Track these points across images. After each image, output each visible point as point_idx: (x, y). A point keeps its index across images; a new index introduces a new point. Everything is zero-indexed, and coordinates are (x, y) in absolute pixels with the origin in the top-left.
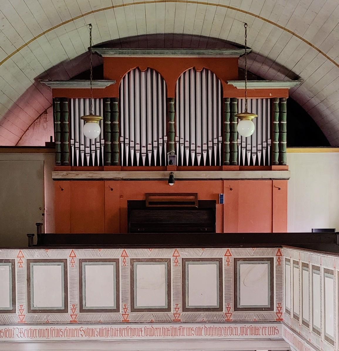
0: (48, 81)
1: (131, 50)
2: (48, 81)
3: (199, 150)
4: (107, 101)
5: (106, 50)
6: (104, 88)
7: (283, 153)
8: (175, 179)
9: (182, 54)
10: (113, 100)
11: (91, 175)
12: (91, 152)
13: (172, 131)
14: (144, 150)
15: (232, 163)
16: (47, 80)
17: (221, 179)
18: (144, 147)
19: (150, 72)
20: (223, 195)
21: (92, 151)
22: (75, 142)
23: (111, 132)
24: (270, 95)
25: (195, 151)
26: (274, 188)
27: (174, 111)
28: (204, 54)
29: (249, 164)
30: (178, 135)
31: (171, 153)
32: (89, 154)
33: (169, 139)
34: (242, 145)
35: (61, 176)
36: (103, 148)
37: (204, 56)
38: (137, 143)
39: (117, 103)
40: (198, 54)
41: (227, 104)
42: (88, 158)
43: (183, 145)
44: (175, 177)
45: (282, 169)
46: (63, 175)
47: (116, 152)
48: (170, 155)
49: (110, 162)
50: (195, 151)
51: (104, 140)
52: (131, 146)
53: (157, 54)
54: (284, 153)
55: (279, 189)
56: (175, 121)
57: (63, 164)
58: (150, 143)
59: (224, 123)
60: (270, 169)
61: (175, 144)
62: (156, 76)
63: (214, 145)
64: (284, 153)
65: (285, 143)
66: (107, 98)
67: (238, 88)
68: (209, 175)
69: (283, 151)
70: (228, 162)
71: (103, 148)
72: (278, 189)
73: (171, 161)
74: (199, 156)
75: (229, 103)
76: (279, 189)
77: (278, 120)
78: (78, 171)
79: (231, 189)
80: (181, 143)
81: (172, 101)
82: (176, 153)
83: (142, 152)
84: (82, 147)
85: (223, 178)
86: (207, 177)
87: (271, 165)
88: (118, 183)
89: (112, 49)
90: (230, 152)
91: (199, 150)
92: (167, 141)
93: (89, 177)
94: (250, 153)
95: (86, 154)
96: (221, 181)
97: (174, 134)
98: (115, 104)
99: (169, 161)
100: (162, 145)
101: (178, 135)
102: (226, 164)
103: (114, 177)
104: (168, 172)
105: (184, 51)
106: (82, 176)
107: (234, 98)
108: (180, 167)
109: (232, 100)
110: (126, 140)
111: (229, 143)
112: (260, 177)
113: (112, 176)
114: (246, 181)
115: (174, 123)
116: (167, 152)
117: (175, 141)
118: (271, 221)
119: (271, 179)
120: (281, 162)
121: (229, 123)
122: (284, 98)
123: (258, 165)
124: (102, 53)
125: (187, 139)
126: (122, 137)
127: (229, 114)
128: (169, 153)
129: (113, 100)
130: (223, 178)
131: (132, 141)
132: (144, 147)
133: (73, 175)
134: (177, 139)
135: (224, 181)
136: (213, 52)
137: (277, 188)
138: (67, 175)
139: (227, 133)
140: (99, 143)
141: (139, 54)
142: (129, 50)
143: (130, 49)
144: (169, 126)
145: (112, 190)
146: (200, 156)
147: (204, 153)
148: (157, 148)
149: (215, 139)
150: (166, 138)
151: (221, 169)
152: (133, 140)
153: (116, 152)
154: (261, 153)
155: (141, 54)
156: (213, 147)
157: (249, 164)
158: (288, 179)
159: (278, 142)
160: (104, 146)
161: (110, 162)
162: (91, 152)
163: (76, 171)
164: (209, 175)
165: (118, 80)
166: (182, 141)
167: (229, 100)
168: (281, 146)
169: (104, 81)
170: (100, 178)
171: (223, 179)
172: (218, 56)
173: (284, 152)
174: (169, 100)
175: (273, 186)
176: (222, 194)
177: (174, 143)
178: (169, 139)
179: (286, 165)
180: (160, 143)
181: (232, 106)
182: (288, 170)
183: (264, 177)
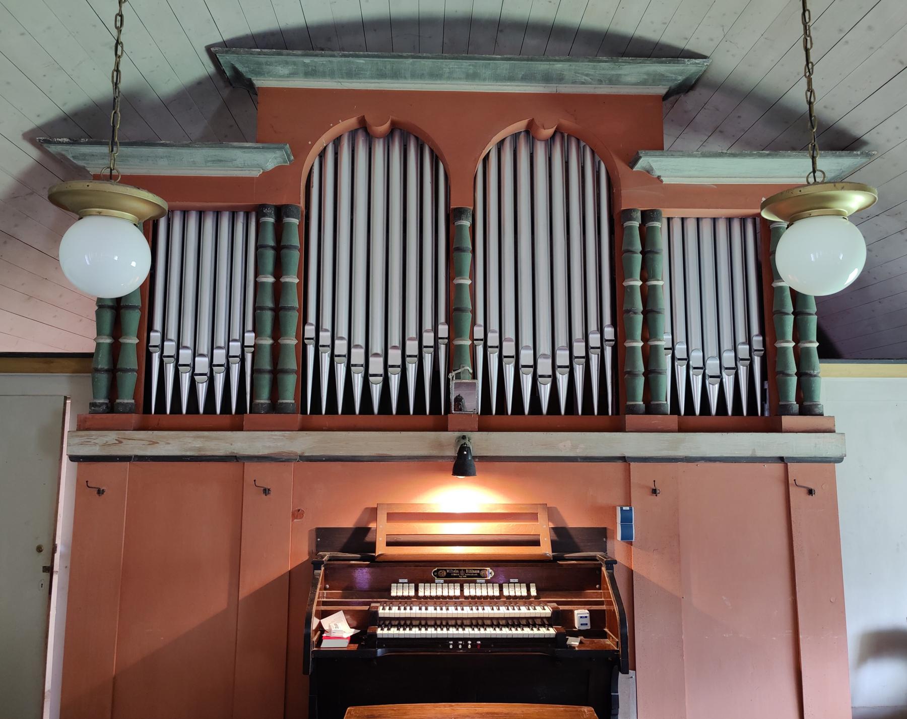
0: (67, 143)
1: (339, 59)
2: (67, 143)
3: (544, 367)
4: (265, 215)
5: (262, 59)
6: (256, 173)
8: (474, 457)
9: (497, 78)
10: (281, 212)
11: (198, 444)
12: (212, 371)
13: (465, 306)
14: (376, 366)
15: (651, 408)
16: (66, 140)
17: (623, 459)
18: (376, 355)
20: (631, 510)
21: (215, 368)
22: (164, 338)
23: (275, 309)
25: (532, 370)
27: (470, 247)
28: (560, 79)
30: (480, 320)
31: (462, 376)
32: (205, 378)
33: (455, 330)
34: (676, 352)
35: (97, 448)
36: (249, 357)
37: (564, 89)
38: (356, 343)
39: (296, 221)
40: (547, 78)
41: (631, 228)
42: (202, 390)
43: (497, 350)
44: (475, 451)
45: (810, 428)
46: (106, 445)
47: (286, 372)
48: (459, 381)
49: (267, 402)
50: (532, 370)
51: (253, 335)
52: (336, 353)
53: (421, 76)
56: (473, 276)
57: (112, 408)
58: (397, 344)
59: (625, 284)
61: (473, 348)
66: (264, 206)
67: (666, 180)
68: (582, 446)
70: (642, 403)
71: (249, 357)
73: (459, 400)
75: (636, 224)
78: (156, 432)
79: (654, 492)
80: (489, 344)
81: (463, 216)
82: (474, 376)
83: (371, 372)
84: (185, 356)
85: (628, 454)
86: (578, 451)
88: (288, 472)
89: (282, 55)
90: (644, 374)
91: (544, 367)
92: (448, 338)
93: (190, 450)
94: (700, 377)
95: (196, 377)
96: (620, 465)
97: (470, 315)
98: (289, 223)
99: (453, 397)
100: (432, 349)
101: (480, 320)
102: (633, 410)
103: (276, 451)
104: (449, 437)
105: (504, 66)
106: (169, 447)
107: (652, 211)
109: (648, 216)
110: (490, 335)
111: (640, 344)
112: (747, 453)
113: (270, 447)
114: (702, 465)
115: (469, 282)
116: (448, 370)
117: (473, 339)
119: (781, 459)
120: (807, 407)
121: (639, 283)
124: (254, 72)
125: (359, 338)
126: (311, 324)
127: (639, 257)
128: (454, 373)
129: (281, 212)
130: (627, 455)
131: (342, 338)
132: (376, 355)
133: (138, 443)
134: (479, 332)
136: (591, 72)
137: (802, 492)
138: (121, 442)
139: (635, 313)
140: (239, 344)
141: (365, 78)
142: (333, 56)
143: (335, 53)
144: (453, 291)
145: (266, 491)
146: (549, 386)
147: (559, 376)
148: (416, 359)
149: (593, 333)
150: (443, 330)
151: (619, 428)
152: (345, 335)
153: (286, 372)
154: (732, 378)
155: (372, 77)
156: (587, 358)
157: (698, 411)
158: (840, 460)
159: (793, 344)
161: (267, 402)
162: (212, 371)
163: (150, 432)
164: (582, 446)
165: (299, 151)
166: (493, 339)
168: (801, 356)
169: (249, 148)
170: (228, 453)
171: (629, 457)
172: (604, 90)
174: (453, 215)
175: (791, 481)
177: (469, 342)
178: (455, 330)
179: (822, 415)
180: (408, 352)
181: (647, 235)
182: (832, 431)
183: (760, 453)
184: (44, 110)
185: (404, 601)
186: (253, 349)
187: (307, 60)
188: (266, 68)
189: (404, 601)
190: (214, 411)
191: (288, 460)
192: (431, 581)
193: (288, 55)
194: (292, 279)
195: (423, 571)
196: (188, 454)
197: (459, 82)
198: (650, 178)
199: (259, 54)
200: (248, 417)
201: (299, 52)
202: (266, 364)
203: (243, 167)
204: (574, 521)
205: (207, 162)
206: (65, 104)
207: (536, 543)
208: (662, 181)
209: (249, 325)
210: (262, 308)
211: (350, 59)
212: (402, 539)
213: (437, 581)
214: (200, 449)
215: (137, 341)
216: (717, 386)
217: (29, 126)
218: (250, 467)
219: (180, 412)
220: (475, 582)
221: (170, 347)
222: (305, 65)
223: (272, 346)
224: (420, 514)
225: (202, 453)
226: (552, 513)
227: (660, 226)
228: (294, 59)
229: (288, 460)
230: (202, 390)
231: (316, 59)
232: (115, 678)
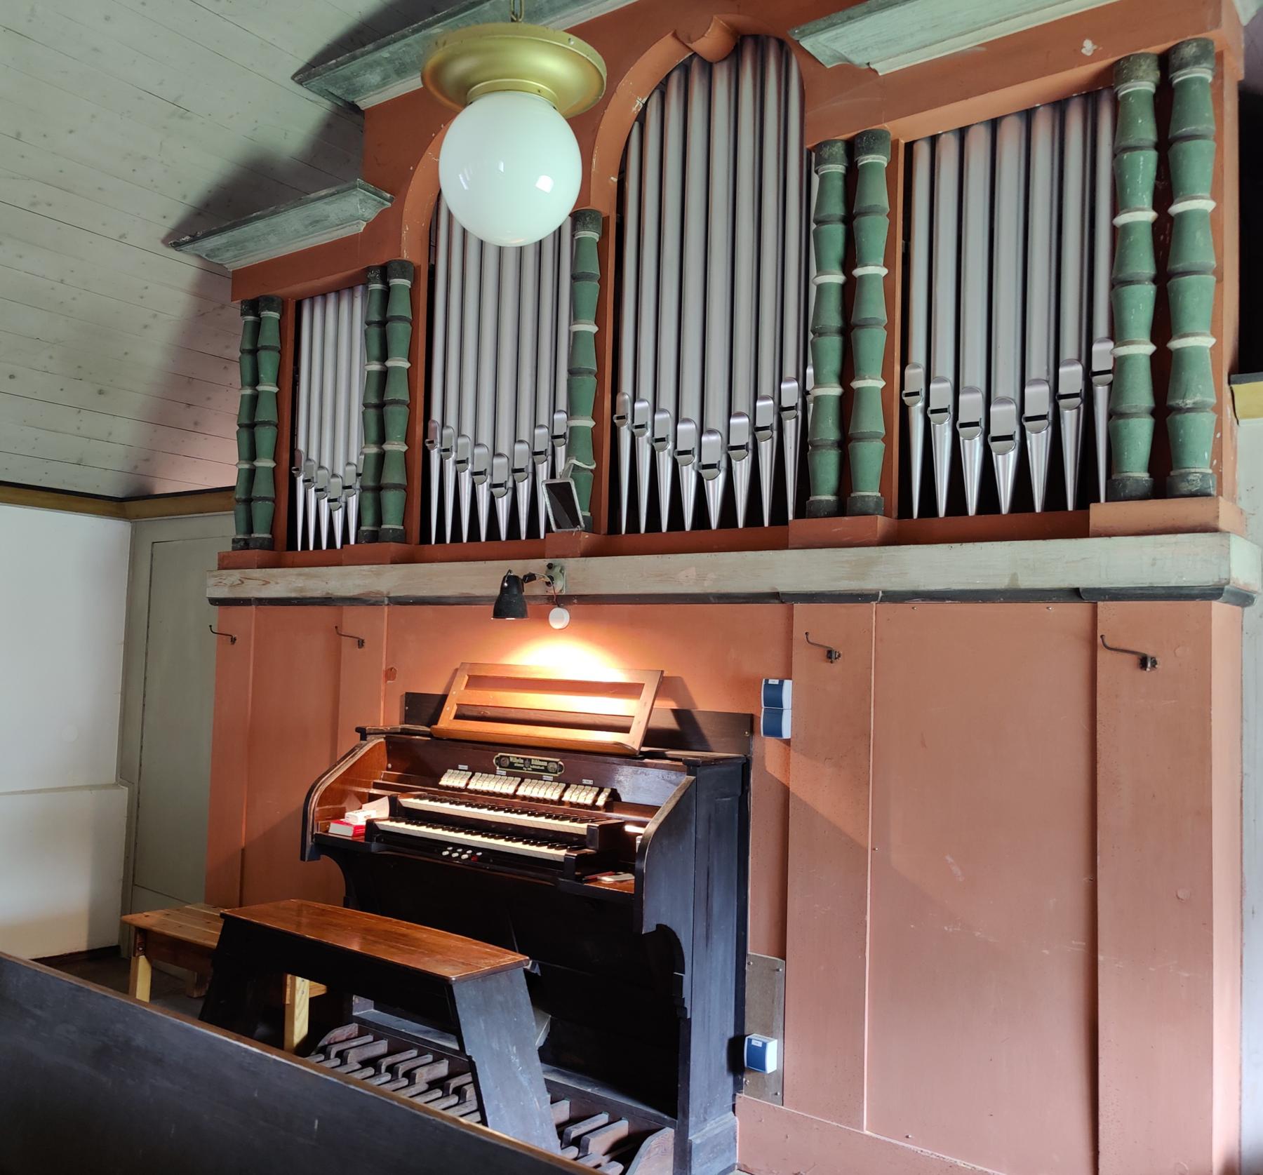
5: (345, 71)
7: (1178, 417)
15: (844, 504)
17: (776, 597)
19: (679, 81)
24: (1088, 47)
26: (1102, 655)
29: (972, 507)
35: (226, 589)
36: (1101, 393)
42: (503, 506)
45: (1157, 523)
54: (1189, 410)
55: (1143, 662)
60: (1079, 529)
62: (755, 86)
63: (1095, 379)
64: (1189, 410)
65: (1208, 337)
67: (883, 68)
68: (712, 576)
69: (1180, 402)
72: (1133, 660)
74: (1004, 453)
76: (1143, 662)
77: (1146, 198)
86: (706, 584)
87: (1087, 493)
93: (295, 590)
106: (278, 587)
108: (427, 546)
112: (1001, 583)
118: (1085, 880)
119: (1076, 594)
122: (1188, 42)
123: (499, 539)
130: (781, 589)
135: (798, 607)
157: (972, 507)
159: (1150, 348)
160: (1110, 384)
164: (712, 576)
167: (839, 150)
171: (784, 594)
173: (1189, 402)
176: (776, 682)
182: (1215, 530)
183: (1026, 582)
184: (172, 210)
185: (455, 795)
186: (1110, 377)
187: (385, 53)
188: (358, 81)
189: (455, 795)
190: (707, 525)
191: (377, 603)
192: (491, 771)
193: (363, 55)
194: (873, 270)
195: (482, 755)
196: (293, 595)
197: (569, 11)
198: (852, 75)
199: (337, 65)
200: (1101, 512)
201: (370, 47)
202: (828, 430)
203: (342, 223)
204: (708, 701)
205: (306, 227)
206: (185, 197)
207: (626, 730)
208: (875, 71)
209: (562, 403)
210: (819, 333)
211: (423, 32)
212: (489, 713)
213: (545, 777)
214: (302, 590)
215: (404, 448)
216: (1012, 456)
217: (163, 233)
218: (350, 613)
219: (638, 530)
220: (540, 778)
221: (941, 393)
222: (389, 60)
223: (1153, 358)
224: (511, 679)
225: (309, 594)
226: (666, 687)
227: (877, 160)
228: (370, 58)
229: (377, 603)
230: (503, 506)
231: (391, 48)
232: (243, 850)
